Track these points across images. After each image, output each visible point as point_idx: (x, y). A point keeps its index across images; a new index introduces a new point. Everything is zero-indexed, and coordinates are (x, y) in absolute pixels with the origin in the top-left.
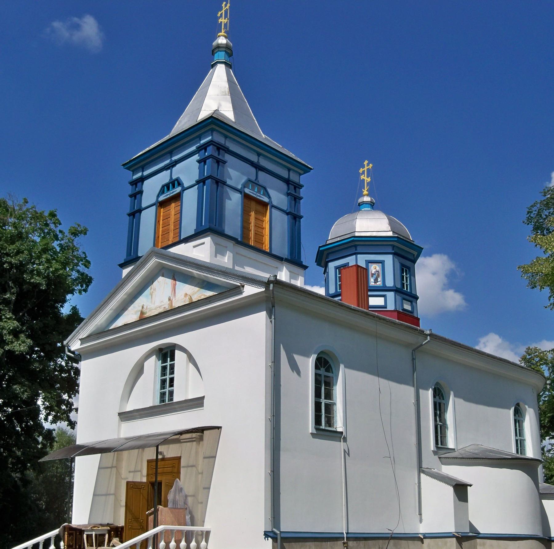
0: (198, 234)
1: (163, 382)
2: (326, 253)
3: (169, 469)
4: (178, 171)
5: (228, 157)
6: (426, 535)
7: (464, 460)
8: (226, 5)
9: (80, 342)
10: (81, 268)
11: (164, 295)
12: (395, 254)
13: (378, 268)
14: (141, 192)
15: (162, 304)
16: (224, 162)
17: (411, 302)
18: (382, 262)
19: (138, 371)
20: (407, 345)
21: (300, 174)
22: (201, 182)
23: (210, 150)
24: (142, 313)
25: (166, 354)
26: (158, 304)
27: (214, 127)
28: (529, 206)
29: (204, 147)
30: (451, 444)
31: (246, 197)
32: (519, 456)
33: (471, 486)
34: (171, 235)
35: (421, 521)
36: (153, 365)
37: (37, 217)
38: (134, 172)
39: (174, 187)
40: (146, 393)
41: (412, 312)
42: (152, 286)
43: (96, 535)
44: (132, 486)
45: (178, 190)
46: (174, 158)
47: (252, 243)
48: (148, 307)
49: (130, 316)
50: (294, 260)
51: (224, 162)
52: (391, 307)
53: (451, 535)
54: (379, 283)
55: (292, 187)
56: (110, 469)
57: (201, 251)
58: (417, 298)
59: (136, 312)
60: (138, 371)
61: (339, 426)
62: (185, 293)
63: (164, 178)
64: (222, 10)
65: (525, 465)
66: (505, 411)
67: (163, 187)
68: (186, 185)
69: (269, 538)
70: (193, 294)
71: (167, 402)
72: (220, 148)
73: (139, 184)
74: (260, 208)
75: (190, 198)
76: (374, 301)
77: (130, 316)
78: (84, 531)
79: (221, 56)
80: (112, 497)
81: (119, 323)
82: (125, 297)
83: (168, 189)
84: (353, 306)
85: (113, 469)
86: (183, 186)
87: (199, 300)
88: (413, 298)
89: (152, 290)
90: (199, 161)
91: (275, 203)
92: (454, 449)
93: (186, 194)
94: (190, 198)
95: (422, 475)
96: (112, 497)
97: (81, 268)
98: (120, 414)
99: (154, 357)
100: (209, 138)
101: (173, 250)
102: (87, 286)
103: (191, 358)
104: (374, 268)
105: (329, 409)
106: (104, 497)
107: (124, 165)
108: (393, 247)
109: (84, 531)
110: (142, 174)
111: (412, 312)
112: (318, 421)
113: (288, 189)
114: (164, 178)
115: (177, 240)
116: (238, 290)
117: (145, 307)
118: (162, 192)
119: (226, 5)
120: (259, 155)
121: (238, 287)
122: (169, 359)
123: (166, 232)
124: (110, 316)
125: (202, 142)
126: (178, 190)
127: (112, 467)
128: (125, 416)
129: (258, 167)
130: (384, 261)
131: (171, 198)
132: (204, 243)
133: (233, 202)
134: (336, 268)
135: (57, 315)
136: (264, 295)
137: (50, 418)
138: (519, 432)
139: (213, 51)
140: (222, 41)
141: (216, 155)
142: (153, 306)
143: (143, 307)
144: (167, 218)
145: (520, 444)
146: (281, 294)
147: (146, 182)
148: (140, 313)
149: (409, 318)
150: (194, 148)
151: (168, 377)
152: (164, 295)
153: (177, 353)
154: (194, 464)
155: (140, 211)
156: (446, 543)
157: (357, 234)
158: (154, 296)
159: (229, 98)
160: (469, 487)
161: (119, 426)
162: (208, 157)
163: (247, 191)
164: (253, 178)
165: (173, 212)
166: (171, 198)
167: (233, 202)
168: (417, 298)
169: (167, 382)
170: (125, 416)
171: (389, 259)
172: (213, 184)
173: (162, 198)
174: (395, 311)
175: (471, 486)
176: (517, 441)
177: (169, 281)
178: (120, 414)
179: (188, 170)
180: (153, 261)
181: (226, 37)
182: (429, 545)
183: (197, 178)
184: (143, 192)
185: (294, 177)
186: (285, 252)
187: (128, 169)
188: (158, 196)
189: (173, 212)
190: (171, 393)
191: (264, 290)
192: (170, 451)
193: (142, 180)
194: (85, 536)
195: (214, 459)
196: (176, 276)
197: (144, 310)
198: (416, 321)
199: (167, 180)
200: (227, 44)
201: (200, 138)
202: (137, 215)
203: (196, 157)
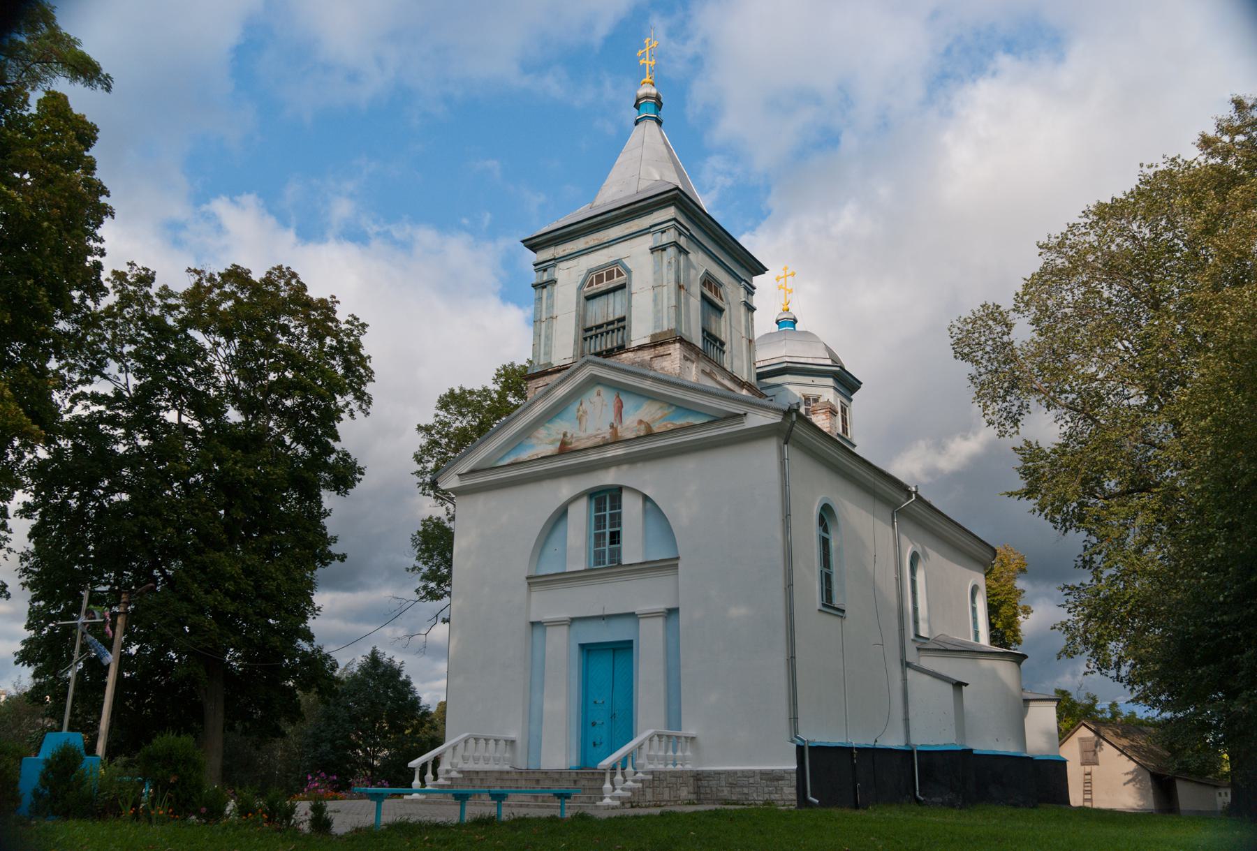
1: (599, 538)
19: (562, 514)
24: (563, 443)
26: (591, 431)
33: (966, 685)
36: (580, 515)
60: (562, 514)
61: (837, 602)
71: (607, 564)
95: (911, 673)
135: (133, 499)
139: (638, 100)
142: (583, 435)
143: (565, 435)
146: (799, 430)
148: (558, 444)
169: (608, 535)
170: (534, 581)
175: (966, 685)
197: (568, 439)
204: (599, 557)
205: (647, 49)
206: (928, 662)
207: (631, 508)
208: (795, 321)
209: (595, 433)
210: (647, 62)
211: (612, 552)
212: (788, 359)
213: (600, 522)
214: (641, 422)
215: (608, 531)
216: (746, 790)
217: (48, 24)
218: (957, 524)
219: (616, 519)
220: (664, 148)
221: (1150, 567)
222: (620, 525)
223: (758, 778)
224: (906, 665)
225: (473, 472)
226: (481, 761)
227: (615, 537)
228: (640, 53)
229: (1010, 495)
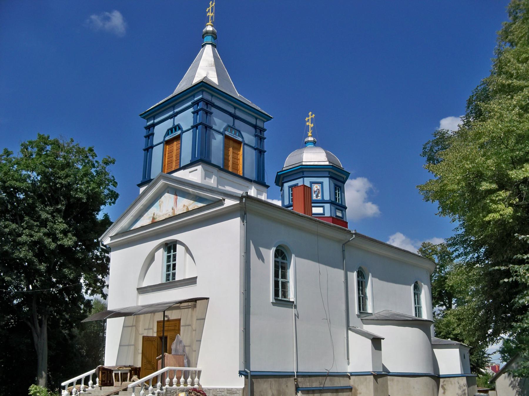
1: (168, 267)
2: (282, 176)
4: (178, 120)
5: (213, 110)
8: (212, 4)
9: (110, 239)
10: (111, 187)
11: (168, 206)
12: (330, 177)
13: (318, 187)
14: (153, 134)
16: (211, 113)
17: (342, 211)
18: (321, 183)
19: (151, 259)
20: (339, 241)
21: (264, 122)
22: (195, 127)
23: (201, 105)
24: (153, 219)
25: (170, 247)
26: (164, 212)
27: (204, 88)
29: (197, 103)
30: (369, 310)
31: (227, 137)
32: (417, 318)
33: (383, 339)
34: (174, 164)
36: (161, 255)
37: (80, 151)
39: (176, 130)
40: (156, 274)
41: (342, 218)
43: (121, 373)
45: (179, 132)
47: (230, 170)
49: (145, 221)
50: (260, 182)
51: (211, 113)
52: (327, 214)
54: (320, 198)
55: (258, 131)
57: (195, 175)
58: (346, 208)
60: (151, 259)
61: (291, 297)
62: (184, 204)
63: (169, 124)
65: (422, 325)
67: (168, 130)
68: (184, 129)
72: (208, 103)
73: (151, 129)
74: (236, 145)
75: (187, 139)
76: (315, 210)
77: (145, 221)
79: (208, 39)
80: (132, 347)
81: (138, 225)
82: (142, 207)
83: (172, 132)
84: (302, 214)
86: (182, 130)
88: (343, 208)
90: (193, 113)
91: (246, 142)
93: (184, 135)
94: (187, 139)
96: (132, 347)
97: (111, 187)
98: (138, 289)
99: (162, 249)
101: (175, 175)
102: (115, 200)
103: (188, 250)
104: (315, 187)
105: (285, 285)
106: (127, 347)
107: (140, 115)
108: (329, 172)
111: (342, 218)
112: (276, 294)
113: (256, 132)
114: (169, 124)
115: (178, 167)
116: (220, 202)
117: (155, 214)
118: (167, 134)
119: (212, 4)
120: (235, 108)
121: (221, 200)
124: (131, 221)
125: (196, 99)
126: (179, 132)
127: (132, 326)
128: (142, 291)
129: (235, 117)
131: (174, 138)
132: (196, 170)
133: (217, 141)
134: (289, 187)
137: (89, 292)
138: (417, 301)
140: (209, 28)
141: (205, 108)
142: (161, 214)
143: (154, 214)
144: (171, 152)
145: (418, 310)
149: (340, 222)
150: (189, 103)
151: (172, 263)
152: (168, 206)
153: (178, 247)
155: (152, 147)
156: (366, 379)
157: (304, 164)
159: (214, 68)
162: (200, 110)
163: (227, 133)
164: (231, 125)
165: (175, 148)
166: (174, 138)
167: (217, 141)
168: (346, 208)
170: (142, 291)
171: (326, 181)
172: (203, 128)
173: (167, 138)
174: (331, 217)
176: (416, 308)
177: (173, 196)
178: (138, 289)
179: (186, 119)
180: (162, 182)
181: (212, 26)
182: (354, 381)
183: (192, 124)
185: (260, 124)
186: (253, 177)
187: (144, 118)
188: (165, 137)
189: (175, 148)
190: (174, 275)
192: (173, 315)
193: (154, 125)
196: (177, 192)
197: (155, 217)
198: (345, 224)
199: (171, 126)
200: (213, 31)
202: (150, 150)
203: (192, 110)
205: (210, 8)
210: (310, 124)
217: (314, 143)
224: (348, 328)
225: (117, 236)
229: (344, 258)
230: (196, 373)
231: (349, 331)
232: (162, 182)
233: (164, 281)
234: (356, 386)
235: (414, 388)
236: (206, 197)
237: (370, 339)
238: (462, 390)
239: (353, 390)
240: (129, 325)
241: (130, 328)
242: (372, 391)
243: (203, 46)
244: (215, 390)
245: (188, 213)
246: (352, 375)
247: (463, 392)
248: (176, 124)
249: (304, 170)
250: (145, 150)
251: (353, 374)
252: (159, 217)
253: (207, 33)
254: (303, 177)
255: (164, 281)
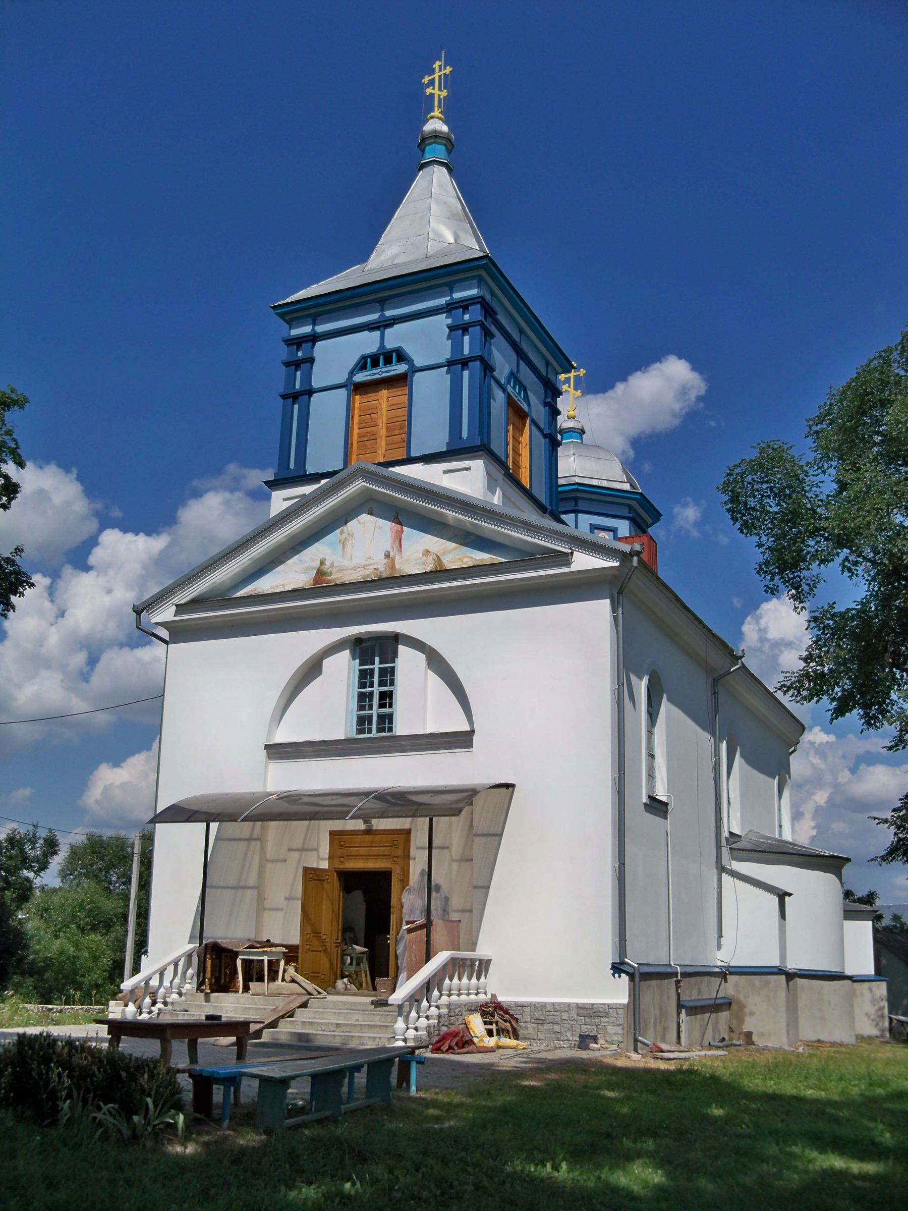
0: (455, 451)
1: (364, 699)
3: (386, 850)
4: (394, 337)
5: (493, 329)
6: (731, 970)
7: (765, 855)
9: (174, 608)
11: (365, 547)
15: (370, 561)
19: (311, 670)
22: (457, 363)
24: (320, 573)
25: (375, 653)
27: (483, 273)
28: (731, 466)
29: (464, 305)
31: (511, 403)
33: (790, 895)
35: (719, 946)
36: (342, 669)
38: (291, 323)
40: (329, 705)
42: (345, 528)
43: (269, 961)
44: (311, 875)
45: (402, 368)
46: (389, 313)
48: (336, 564)
49: (292, 575)
53: (776, 970)
56: (246, 843)
59: (306, 570)
60: (311, 670)
62: (420, 551)
63: (368, 342)
64: (434, 73)
66: (770, 780)
67: (364, 358)
69: (623, 975)
70: (444, 554)
77: (292, 575)
78: (236, 954)
79: (436, 151)
80: (250, 894)
81: (266, 584)
82: (284, 540)
85: (253, 843)
87: (473, 567)
89: (345, 535)
91: (534, 415)
92: (740, 836)
95: (723, 874)
96: (250, 894)
98: (267, 747)
99: (346, 653)
100: (474, 292)
102: (10, 500)
106: (230, 892)
107: (274, 308)
108: (630, 507)
109: (236, 954)
110: (313, 329)
113: (546, 397)
117: (328, 563)
118: (362, 365)
120: (521, 331)
121: (567, 554)
122: (377, 659)
123: (368, 438)
124: (244, 570)
125: (457, 295)
126: (402, 368)
127: (250, 839)
128: (279, 752)
130: (616, 529)
132: (469, 469)
136: (615, 572)
140: (436, 124)
142: (346, 563)
143: (322, 562)
147: (319, 344)
148: (315, 572)
150: (442, 301)
152: (365, 547)
154: (447, 845)
156: (767, 983)
158: (349, 544)
160: (787, 898)
161: (266, 768)
170: (279, 752)
173: (360, 377)
175: (790, 895)
177: (387, 526)
178: (267, 747)
180: (358, 485)
182: (736, 985)
184: (314, 360)
187: (282, 316)
188: (352, 373)
191: (618, 564)
193: (314, 338)
194: (239, 963)
195: (497, 838)
196: (400, 516)
197: (326, 567)
200: (448, 134)
201: (451, 288)
204: (363, 722)
205: (436, 76)
206: (737, 866)
207: (408, 660)
208: (582, 432)
209: (364, 563)
210: (436, 92)
211: (382, 718)
212: (577, 480)
213: (365, 677)
214: (427, 552)
215: (376, 690)
216: (557, 1028)
218: (794, 717)
219: (388, 676)
220: (460, 206)
221: (837, 697)
222: (392, 683)
223: (573, 1014)
224: (722, 869)
225: (196, 603)
226: (153, 1008)
227: (386, 698)
228: (426, 80)
230: (464, 964)
231: (723, 874)
232: (358, 485)
233: (353, 734)
234: (742, 998)
235: (829, 1003)
236: (499, 539)
237: (774, 894)
238: (877, 1007)
239: (734, 1006)
240: (243, 837)
241: (243, 844)
242: (783, 1009)
243: (422, 166)
244: (534, 1006)
245: (440, 573)
246: (731, 973)
247: (880, 1013)
248: (389, 345)
249: (579, 495)
250: (284, 397)
251: (724, 974)
252: (340, 570)
253: (436, 136)
254: (576, 512)
255: (353, 734)
